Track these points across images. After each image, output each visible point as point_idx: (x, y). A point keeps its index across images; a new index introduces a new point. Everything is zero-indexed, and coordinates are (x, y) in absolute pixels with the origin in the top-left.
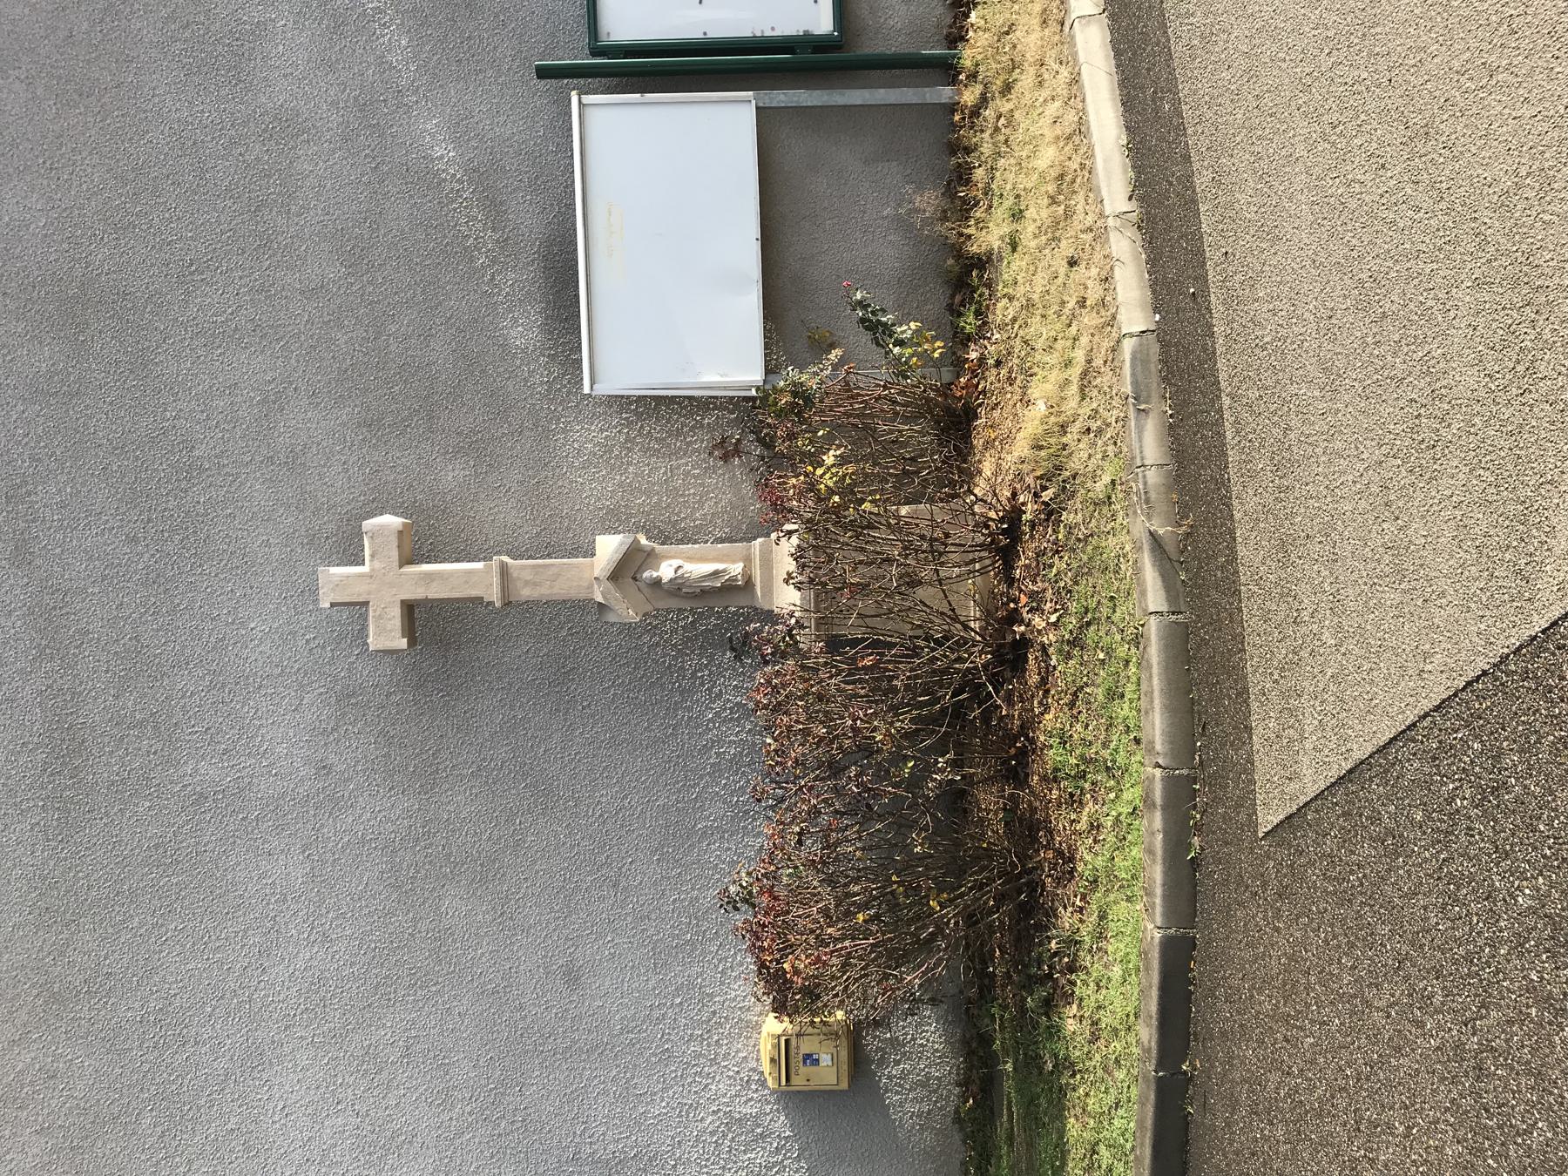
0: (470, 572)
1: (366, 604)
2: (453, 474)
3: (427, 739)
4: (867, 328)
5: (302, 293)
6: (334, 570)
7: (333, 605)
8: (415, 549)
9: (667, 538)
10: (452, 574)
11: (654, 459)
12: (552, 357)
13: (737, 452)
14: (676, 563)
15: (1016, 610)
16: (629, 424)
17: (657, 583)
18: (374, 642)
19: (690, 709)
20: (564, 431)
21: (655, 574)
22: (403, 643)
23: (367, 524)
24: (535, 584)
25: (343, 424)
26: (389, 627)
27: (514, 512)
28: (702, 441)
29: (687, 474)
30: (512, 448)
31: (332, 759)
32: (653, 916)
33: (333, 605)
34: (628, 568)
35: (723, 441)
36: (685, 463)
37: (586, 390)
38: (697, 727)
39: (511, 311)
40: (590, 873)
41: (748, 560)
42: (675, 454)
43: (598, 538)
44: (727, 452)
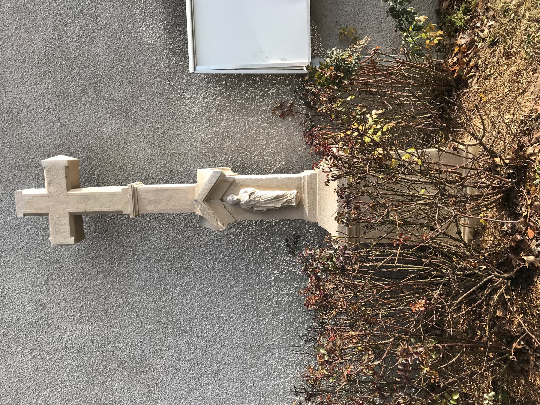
0: (113, 194)
1: (47, 214)
2: (111, 127)
3: (100, 290)
4: (394, 16)
5: (12, 9)
6: (27, 192)
7: (25, 215)
8: (76, 179)
9: (246, 167)
10: (101, 195)
11: (237, 117)
12: (171, 50)
13: (291, 111)
14: (250, 190)
15: (522, 241)
16: (221, 94)
17: (237, 203)
18: (53, 240)
19: (260, 274)
20: (180, 98)
21: (236, 198)
22: (71, 240)
23: (46, 162)
24: (156, 202)
25: (42, 95)
26: (62, 230)
27: (149, 151)
28: (268, 105)
29: (258, 126)
30: (147, 110)
31: (46, 300)
32: (238, 395)
33: (25, 215)
34: (219, 191)
35: (282, 104)
36: (257, 120)
37: (191, 70)
38: (265, 285)
39: (144, 20)
40: (200, 369)
41: (299, 188)
42: (250, 113)
43: (198, 171)
44: (284, 111)
